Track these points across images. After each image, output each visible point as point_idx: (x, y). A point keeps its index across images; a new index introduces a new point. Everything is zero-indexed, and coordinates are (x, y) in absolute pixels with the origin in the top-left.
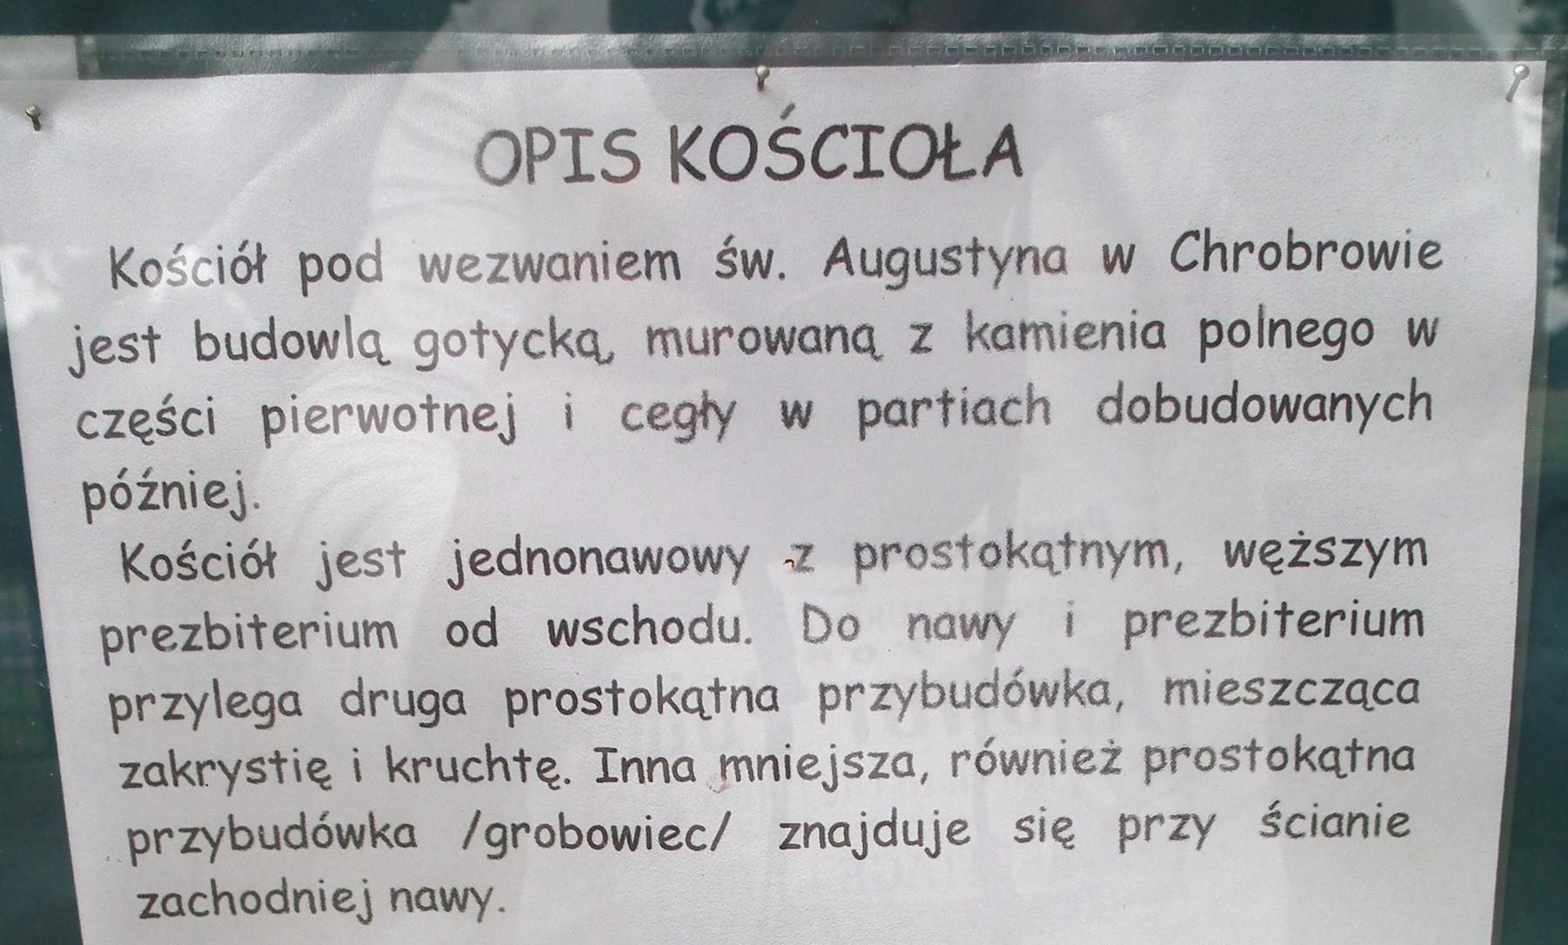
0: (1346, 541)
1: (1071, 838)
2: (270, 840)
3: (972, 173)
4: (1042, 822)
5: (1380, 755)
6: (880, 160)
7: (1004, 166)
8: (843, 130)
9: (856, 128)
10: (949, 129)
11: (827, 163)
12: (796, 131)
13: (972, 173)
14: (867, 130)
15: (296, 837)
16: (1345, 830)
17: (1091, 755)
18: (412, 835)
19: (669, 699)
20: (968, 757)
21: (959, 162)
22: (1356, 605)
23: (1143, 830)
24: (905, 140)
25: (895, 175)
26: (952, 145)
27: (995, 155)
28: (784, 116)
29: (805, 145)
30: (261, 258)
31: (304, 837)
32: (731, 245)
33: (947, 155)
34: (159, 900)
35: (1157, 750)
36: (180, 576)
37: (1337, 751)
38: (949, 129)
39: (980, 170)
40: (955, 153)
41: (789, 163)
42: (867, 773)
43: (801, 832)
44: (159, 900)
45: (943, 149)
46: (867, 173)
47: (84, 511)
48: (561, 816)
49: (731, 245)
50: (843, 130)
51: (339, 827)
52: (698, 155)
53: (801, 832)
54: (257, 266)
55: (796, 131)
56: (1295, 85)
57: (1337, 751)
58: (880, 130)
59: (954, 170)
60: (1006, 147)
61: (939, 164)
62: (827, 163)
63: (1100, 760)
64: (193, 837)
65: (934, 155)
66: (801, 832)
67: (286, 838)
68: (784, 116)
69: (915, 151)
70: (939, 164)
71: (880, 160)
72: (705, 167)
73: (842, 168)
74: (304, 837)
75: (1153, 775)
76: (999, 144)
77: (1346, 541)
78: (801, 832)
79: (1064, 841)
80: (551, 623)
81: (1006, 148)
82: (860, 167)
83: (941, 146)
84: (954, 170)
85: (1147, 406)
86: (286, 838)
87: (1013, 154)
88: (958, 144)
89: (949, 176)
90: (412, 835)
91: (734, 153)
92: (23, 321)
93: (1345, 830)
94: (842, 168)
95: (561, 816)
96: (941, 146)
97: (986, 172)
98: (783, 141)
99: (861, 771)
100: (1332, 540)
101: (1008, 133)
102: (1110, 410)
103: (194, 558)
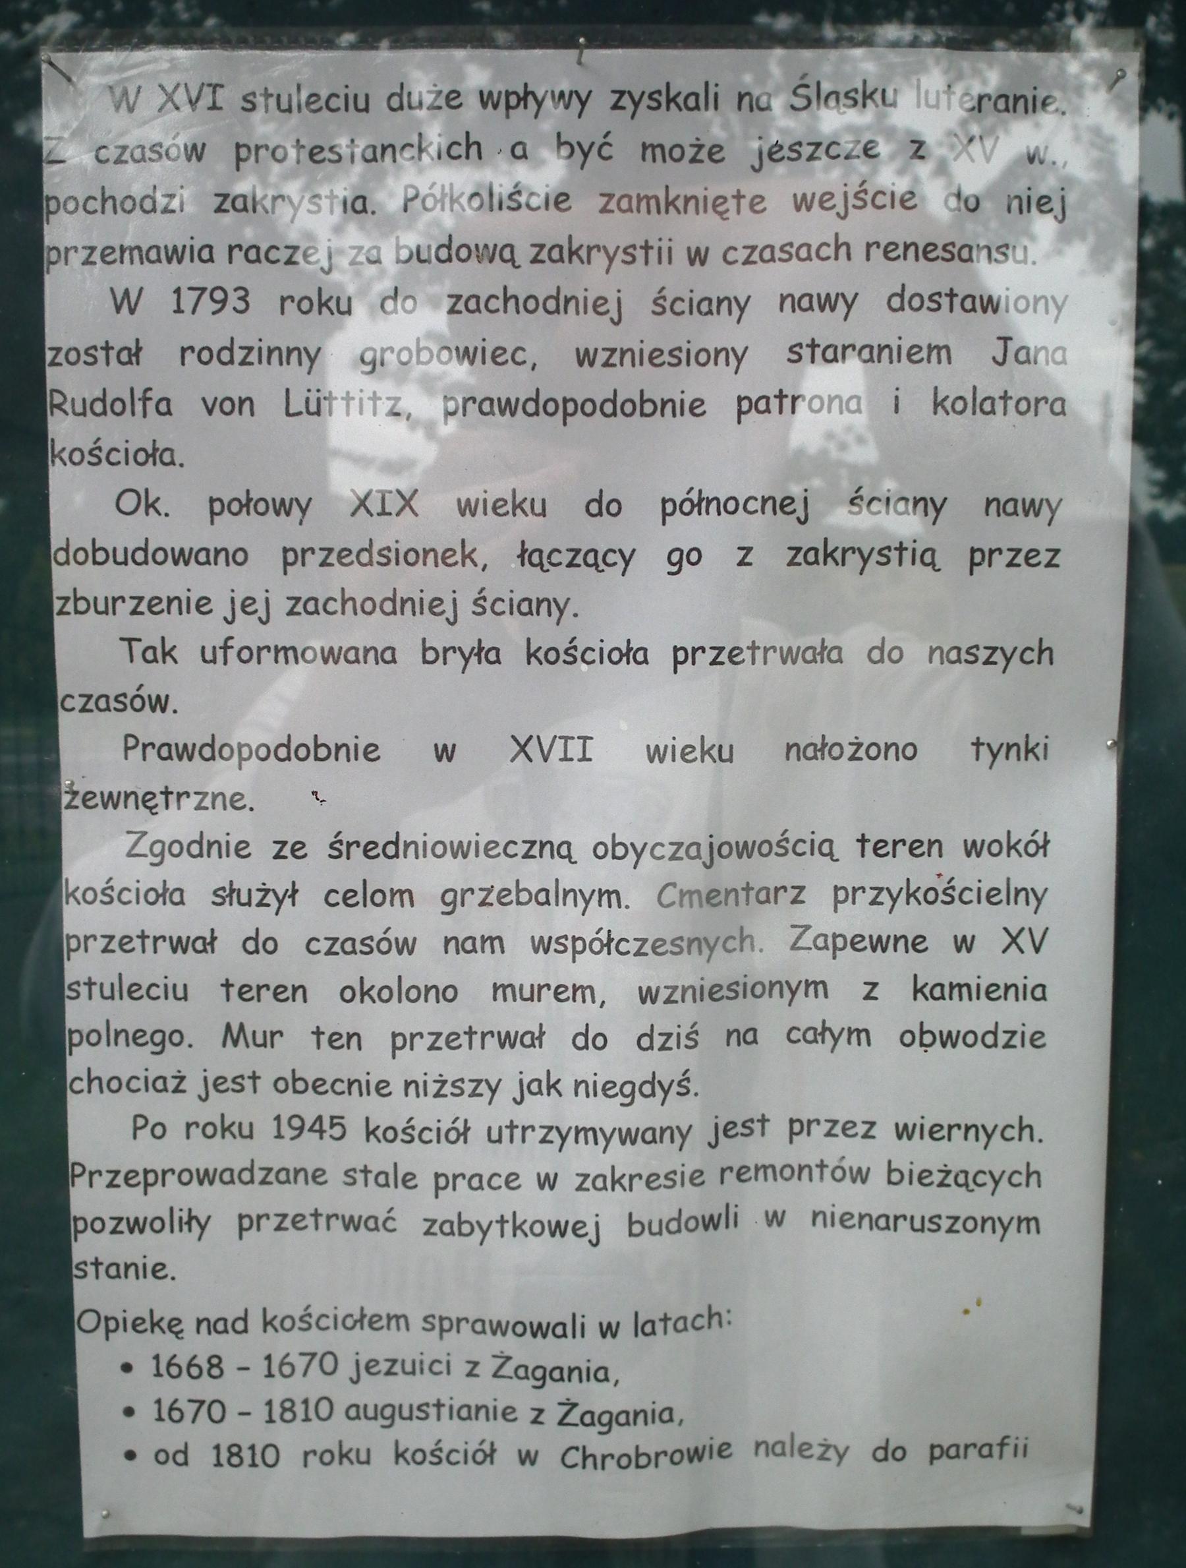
2: (120, 558)
5: (453, 942)
15: (282, 752)
16: (473, 1416)
17: (1038, 553)
18: (498, 656)
20: (641, 1178)
22: (545, 1168)
30: (493, 1451)
31: (289, 753)
32: (662, 294)
35: (840, 935)
42: (805, 156)
43: (617, 355)
48: (94, 541)
49: (662, 294)
51: (851, 1169)
53: (617, 354)
54: (490, 1455)
63: (1045, 557)
64: (878, 895)
66: (617, 355)
67: (92, 408)
74: (289, 753)
75: (440, 1192)
78: (617, 354)
80: (539, 1175)
86: (92, 408)
90: (498, 656)
93: (473, 1416)
95: (94, 541)
99: (688, 1092)
103: (665, 300)
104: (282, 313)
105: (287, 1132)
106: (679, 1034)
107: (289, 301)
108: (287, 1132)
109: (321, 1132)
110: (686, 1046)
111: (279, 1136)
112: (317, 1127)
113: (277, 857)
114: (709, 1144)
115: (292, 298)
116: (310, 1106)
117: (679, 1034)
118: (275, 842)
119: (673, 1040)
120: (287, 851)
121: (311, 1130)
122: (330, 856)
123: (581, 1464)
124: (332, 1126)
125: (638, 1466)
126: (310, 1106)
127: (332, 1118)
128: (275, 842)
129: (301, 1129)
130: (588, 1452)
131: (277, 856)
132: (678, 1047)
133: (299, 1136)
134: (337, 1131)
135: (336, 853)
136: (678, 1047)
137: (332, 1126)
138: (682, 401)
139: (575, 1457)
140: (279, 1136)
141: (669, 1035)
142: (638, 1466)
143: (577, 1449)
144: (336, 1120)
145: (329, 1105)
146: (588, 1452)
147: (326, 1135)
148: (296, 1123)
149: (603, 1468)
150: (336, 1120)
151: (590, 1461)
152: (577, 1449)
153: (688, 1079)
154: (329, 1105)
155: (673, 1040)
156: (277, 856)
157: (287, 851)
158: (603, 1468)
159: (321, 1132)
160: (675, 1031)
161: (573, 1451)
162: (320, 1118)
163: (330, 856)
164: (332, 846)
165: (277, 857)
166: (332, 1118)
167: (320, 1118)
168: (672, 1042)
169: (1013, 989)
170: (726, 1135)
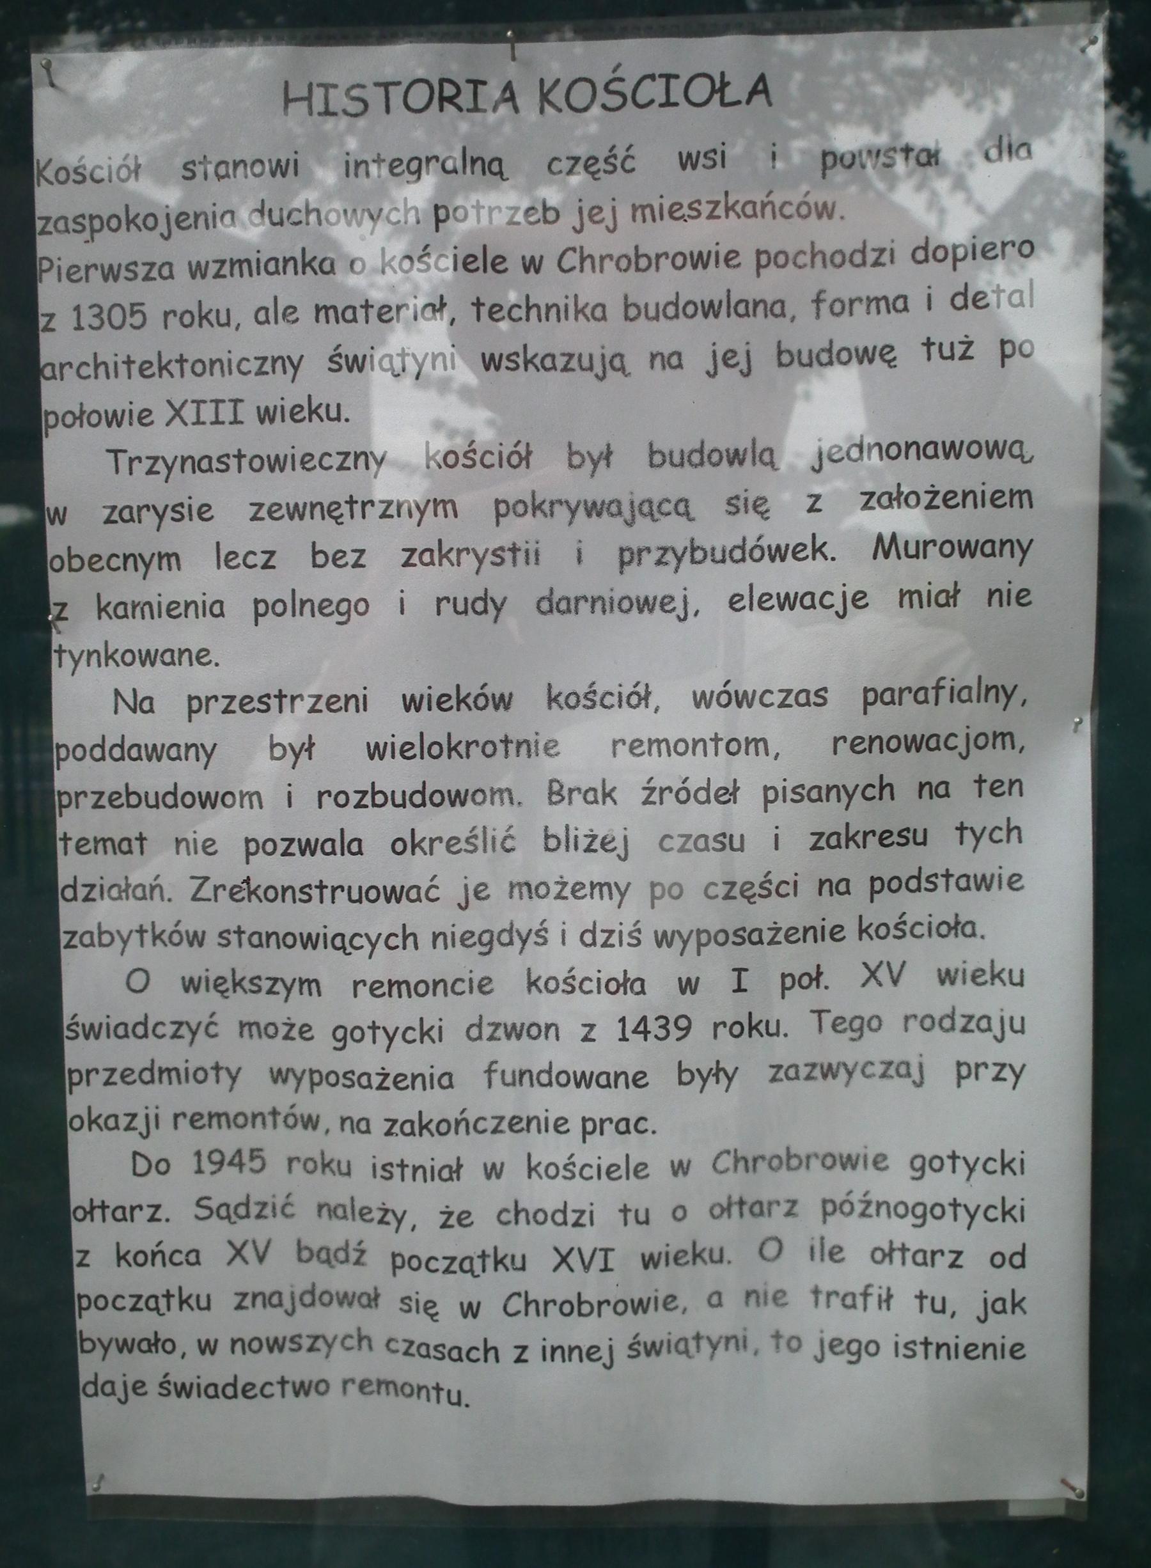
0: (144, 264)
1: (767, 511)
3: (739, 102)
4: (746, 500)
6: (677, 95)
7: (760, 99)
8: (652, 77)
9: (661, 76)
10: (723, 74)
11: (641, 99)
12: (622, 80)
13: (739, 102)
14: (668, 77)
19: (133, 221)
21: (731, 94)
23: (686, 458)
24: (694, 82)
25: (687, 104)
26: (725, 84)
27: (754, 92)
28: (614, 71)
29: (627, 88)
33: (722, 90)
34: (399, 1124)
36: (464, 465)
37: (354, 308)
38: (723, 74)
39: (744, 101)
40: (727, 90)
41: (618, 101)
44: (399, 1124)
45: (720, 88)
46: (668, 104)
47: (1027, 1252)
50: (652, 77)
52: (558, 96)
55: (622, 80)
56: (440, 215)
57: (354, 308)
58: (677, 77)
59: (727, 100)
60: (760, 87)
61: (717, 97)
62: (641, 99)
65: (713, 91)
68: (614, 71)
69: (700, 90)
70: (717, 97)
71: (677, 95)
72: (562, 104)
73: (652, 101)
76: (756, 85)
77: (144, 264)
79: (762, 513)
81: (760, 87)
82: (663, 100)
83: (718, 85)
84: (727, 100)
85: (629, 261)
87: (766, 91)
88: (728, 83)
89: (723, 104)
91: (581, 95)
92: (186, 41)
94: (652, 101)
96: (718, 85)
97: (748, 102)
98: (614, 86)
100: (135, 264)
101: (762, 78)
102: (920, 255)
104: (166, 327)
105: (207, 1167)
106: (621, 932)
107: (172, 315)
108: (207, 1167)
109: (241, 1165)
110: (629, 944)
111: (199, 1171)
112: (236, 1160)
113: (254, 518)
114: (708, 373)
115: (174, 312)
116: (228, 1140)
117: (621, 932)
118: (252, 504)
119: (615, 936)
120: (263, 513)
121: (231, 1163)
122: (330, 369)
123: (523, 1312)
124: (252, 1158)
125: (580, 1314)
126: (228, 1140)
127: (252, 1151)
128: (252, 504)
129: (221, 1163)
130: (530, 1298)
131: (254, 518)
132: (621, 944)
133: (219, 1170)
134: (257, 1164)
135: (335, 367)
136: (621, 944)
137: (252, 1158)
138: (546, 1119)
139: (517, 1304)
140: (199, 1171)
141: (611, 932)
142: (580, 1314)
143: (519, 1294)
144: (255, 1153)
145: (247, 1138)
146: (530, 1298)
147: (246, 1169)
148: (216, 1157)
149: (546, 1314)
150: (255, 1153)
151: (532, 1307)
152: (519, 1294)
153: (639, 931)
154: (247, 1138)
155: (615, 936)
156: (254, 518)
157: (263, 513)
158: (546, 1314)
159: (241, 1165)
160: (617, 928)
161: (516, 1297)
162: (239, 1152)
163: (330, 369)
164: (331, 360)
165: (254, 518)
166: (252, 1151)
167: (239, 1152)
168: (614, 939)
169: (944, 1348)
170: (726, 364)
